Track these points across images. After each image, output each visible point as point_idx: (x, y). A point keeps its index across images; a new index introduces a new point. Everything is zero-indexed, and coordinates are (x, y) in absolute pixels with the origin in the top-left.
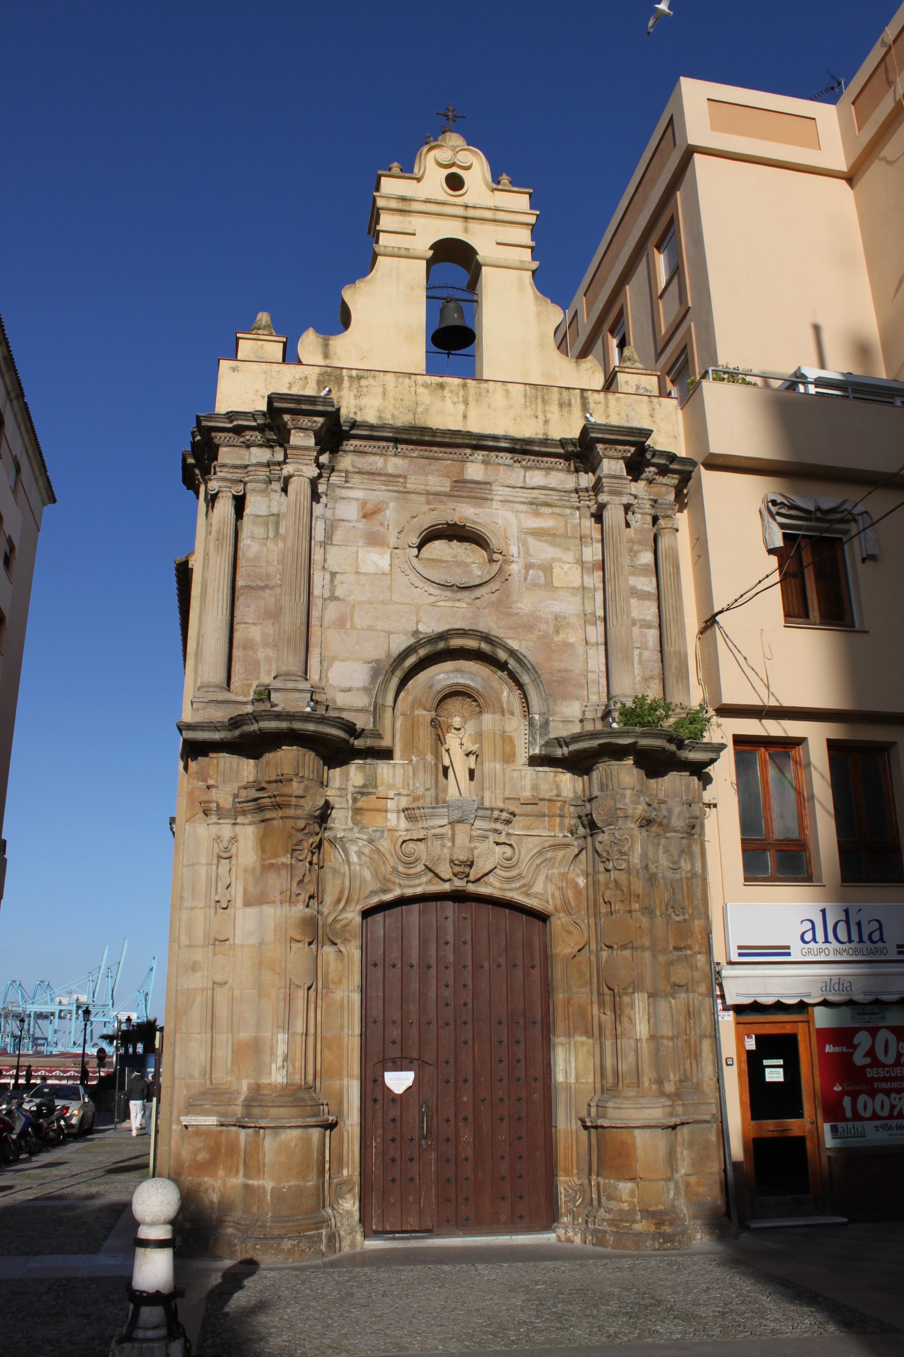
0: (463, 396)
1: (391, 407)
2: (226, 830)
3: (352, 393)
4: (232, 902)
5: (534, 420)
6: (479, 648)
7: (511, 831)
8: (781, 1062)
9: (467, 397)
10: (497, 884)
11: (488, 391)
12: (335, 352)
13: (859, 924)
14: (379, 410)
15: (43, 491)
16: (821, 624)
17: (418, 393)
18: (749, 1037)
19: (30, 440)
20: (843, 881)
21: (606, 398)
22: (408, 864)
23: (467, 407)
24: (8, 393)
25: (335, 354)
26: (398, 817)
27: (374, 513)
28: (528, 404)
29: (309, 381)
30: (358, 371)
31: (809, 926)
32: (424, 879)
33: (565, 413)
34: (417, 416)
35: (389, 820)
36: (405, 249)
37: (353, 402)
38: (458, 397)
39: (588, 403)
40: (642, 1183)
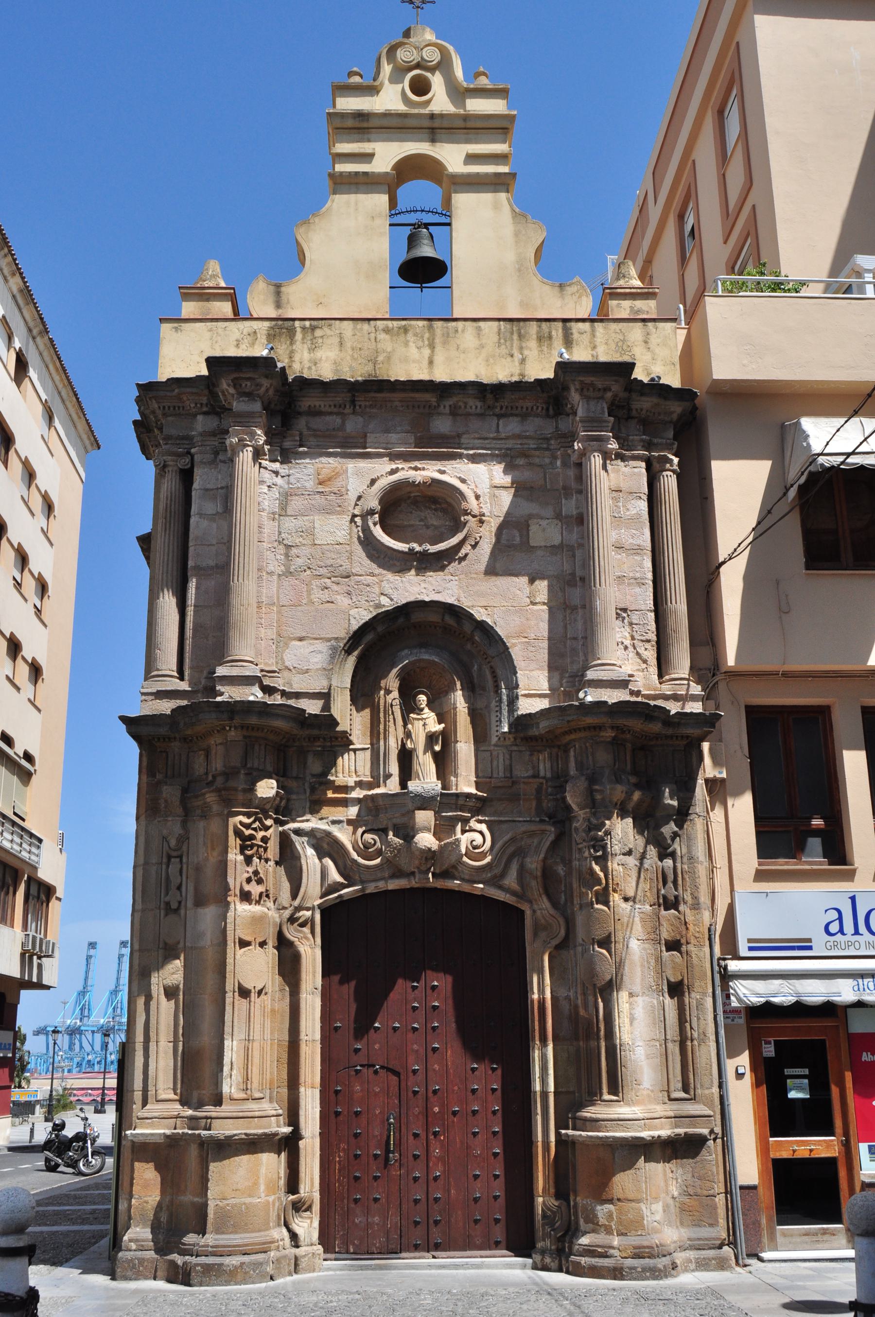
0: (428, 339)
1: (348, 358)
3: (305, 346)
4: (183, 904)
5: (509, 359)
8: (806, 1071)
9: (434, 339)
11: (457, 331)
12: (288, 300)
14: (335, 363)
15: (85, 437)
19: (62, 380)
23: (433, 352)
24: (30, 330)
25: (288, 302)
28: (502, 341)
29: (259, 336)
31: (835, 915)
33: (545, 348)
34: (377, 366)
37: (306, 355)
38: (423, 341)
39: (572, 334)
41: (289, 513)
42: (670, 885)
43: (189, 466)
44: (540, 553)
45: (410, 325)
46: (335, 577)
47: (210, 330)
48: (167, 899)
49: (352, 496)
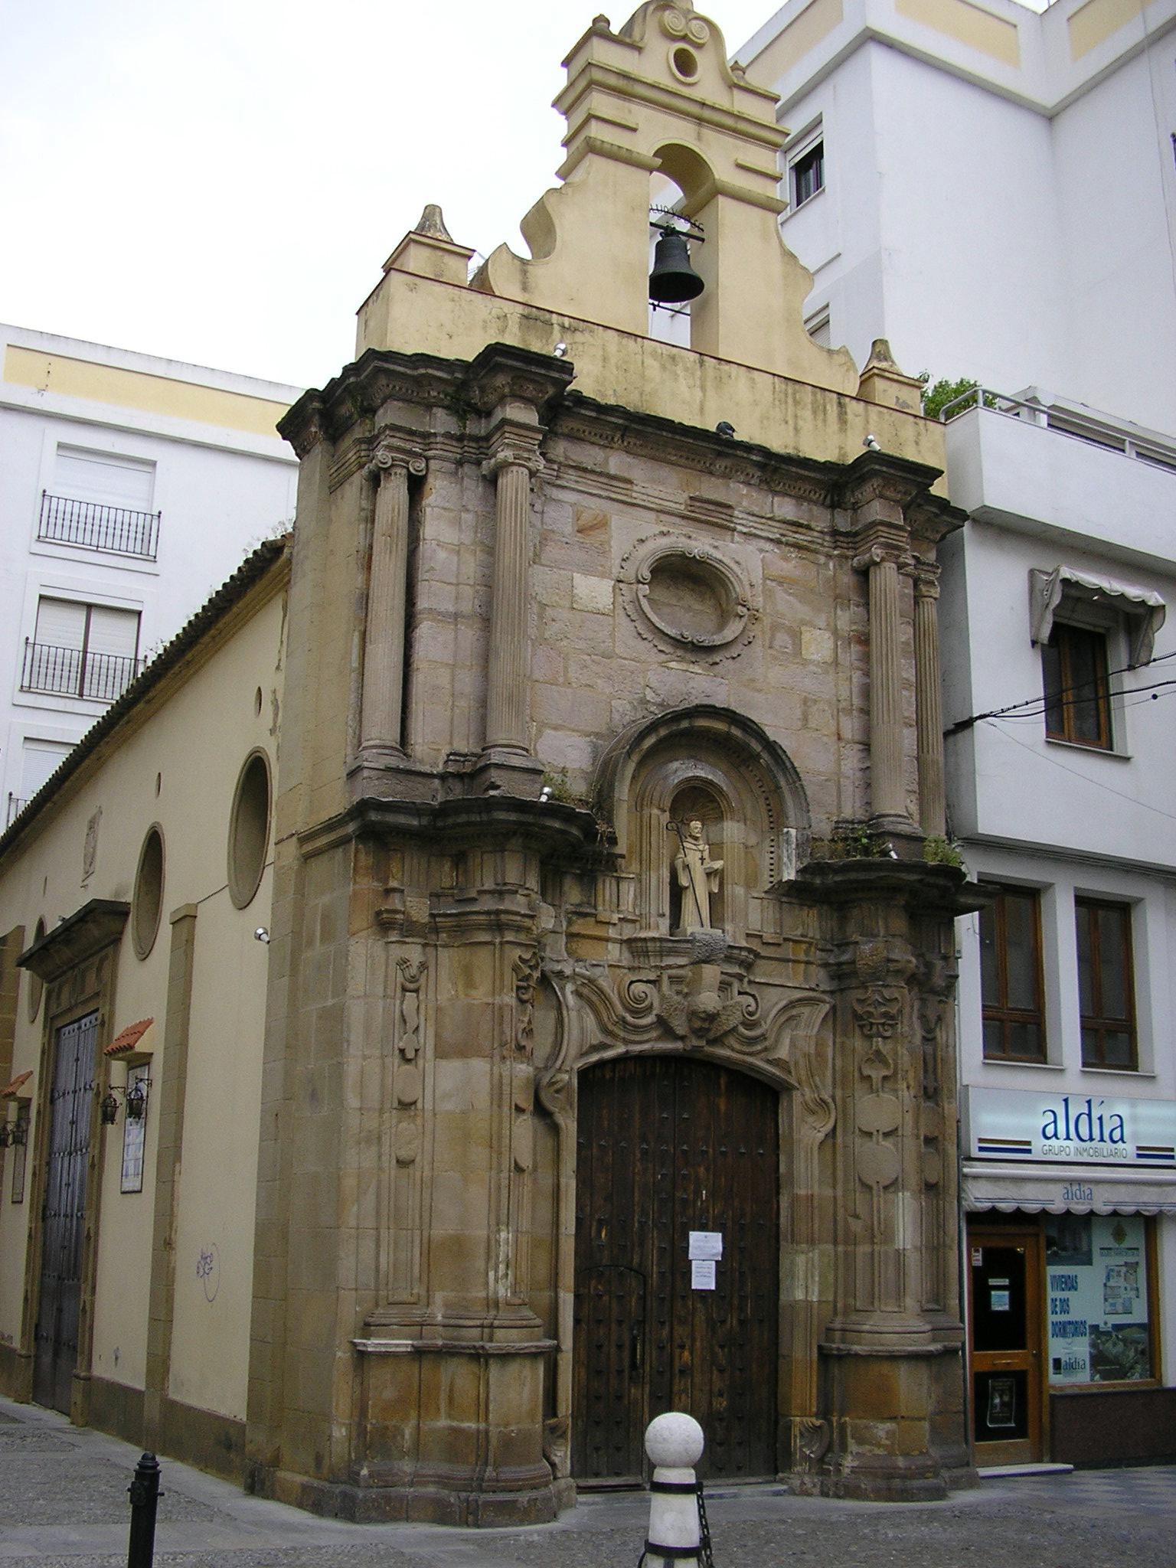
2: (414, 953)
4: (420, 1053)
5: (783, 426)
6: (728, 733)
7: (752, 978)
8: (1006, 1282)
10: (737, 1046)
13: (1100, 1119)
16: (1077, 741)
17: (645, 365)
18: (977, 1251)
20: (1085, 1064)
21: (866, 411)
26: (621, 950)
27: (592, 528)
30: (572, 320)
32: (654, 1034)
35: (609, 952)
36: (627, 150)
40: (903, 1423)
41: (544, 562)
42: (931, 1075)
43: (424, 472)
45: (681, 357)
46: (597, 655)
48: (401, 1045)
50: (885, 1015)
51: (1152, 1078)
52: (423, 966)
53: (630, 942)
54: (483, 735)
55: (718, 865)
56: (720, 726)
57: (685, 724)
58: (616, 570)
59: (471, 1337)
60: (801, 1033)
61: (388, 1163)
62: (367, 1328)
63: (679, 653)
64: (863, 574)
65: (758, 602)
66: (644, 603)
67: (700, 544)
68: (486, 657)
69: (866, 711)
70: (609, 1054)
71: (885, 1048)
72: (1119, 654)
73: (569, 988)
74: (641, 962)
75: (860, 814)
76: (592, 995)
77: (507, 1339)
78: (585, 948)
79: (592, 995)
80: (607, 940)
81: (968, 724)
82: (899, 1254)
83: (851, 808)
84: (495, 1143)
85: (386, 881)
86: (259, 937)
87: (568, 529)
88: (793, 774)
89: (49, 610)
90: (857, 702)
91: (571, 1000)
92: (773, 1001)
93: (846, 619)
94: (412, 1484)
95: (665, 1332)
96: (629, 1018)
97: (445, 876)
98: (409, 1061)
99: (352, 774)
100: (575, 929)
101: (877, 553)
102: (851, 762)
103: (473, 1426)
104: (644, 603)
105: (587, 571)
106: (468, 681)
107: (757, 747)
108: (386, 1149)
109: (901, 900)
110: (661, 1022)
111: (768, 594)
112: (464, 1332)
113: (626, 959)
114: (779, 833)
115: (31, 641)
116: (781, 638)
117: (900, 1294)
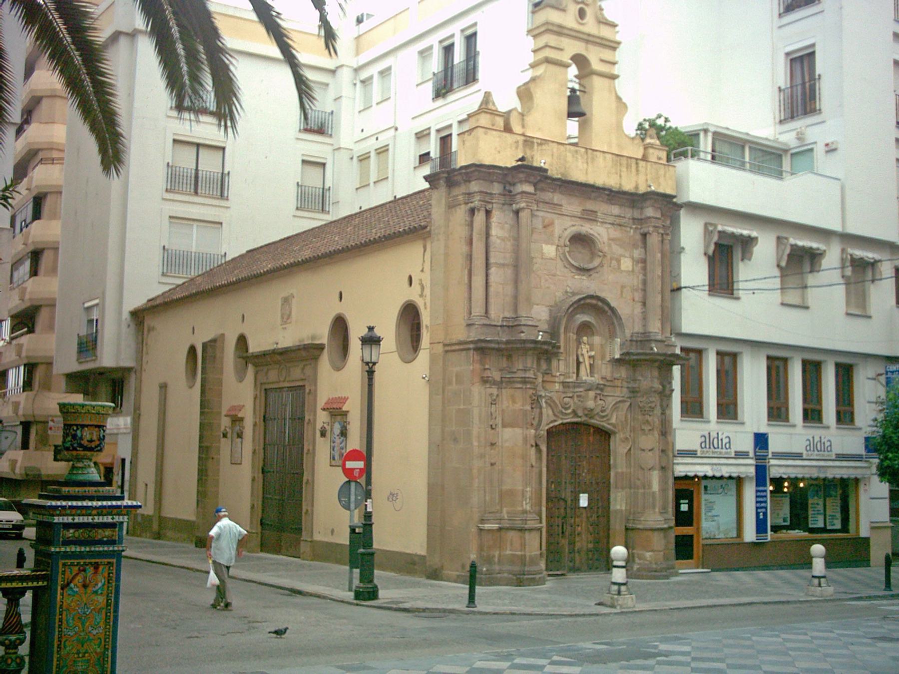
2: (494, 391)
8: (687, 501)
13: (722, 440)
20: (718, 418)
22: (566, 409)
27: (548, 225)
32: (571, 416)
40: (656, 553)
44: (624, 274)
47: (500, 137)
49: (557, 235)
50: (650, 407)
51: (743, 423)
52: (497, 395)
53: (563, 383)
54: (516, 310)
55: (593, 353)
56: (594, 302)
57: (582, 302)
58: (557, 241)
59: (518, 524)
60: (620, 413)
61: (488, 465)
62: (482, 521)
63: (579, 272)
64: (644, 235)
65: (606, 249)
66: (567, 254)
67: (586, 228)
68: (516, 282)
69: (644, 290)
70: (556, 423)
71: (650, 419)
72: (737, 254)
73: (544, 400)
74: (566, 390)
75: (641, 331)
76: (551, 403)
77: (531, 524)
78: (548, 386)
79: (551, 403)
80: (555, 382)
81: (679, 289)
82: (654, 493)
83: (638, 328)
84: (524, 457)
85: (484, 365)
86: (424, 378)
87: (541, 227)
88: (619, 318)
89: (179, 147)
90: (640, 286)
91: (544, 405)
92: (611, 401)
93: (638, 253)
94: (499, 573)
95: (573, 521)
96: (564, 411)
97: (504, 363)
98: (493, 429)
99: (469, 325)
100: (545, 379)
101: (651, 229)
102: (638, 309)
103: (520, 553)
104: (567, 254)
105: (547, 243)
106: (510, 289)
107: (606, 308)
108: (487, 460)
109: (657, 364)
110: (574, 412)
111: (610, 246)
112: (517, 522)
113: (561, 388)
114: (613, 340)
115: (170, 164)
116: (614, 263)
117: (654, 507)
